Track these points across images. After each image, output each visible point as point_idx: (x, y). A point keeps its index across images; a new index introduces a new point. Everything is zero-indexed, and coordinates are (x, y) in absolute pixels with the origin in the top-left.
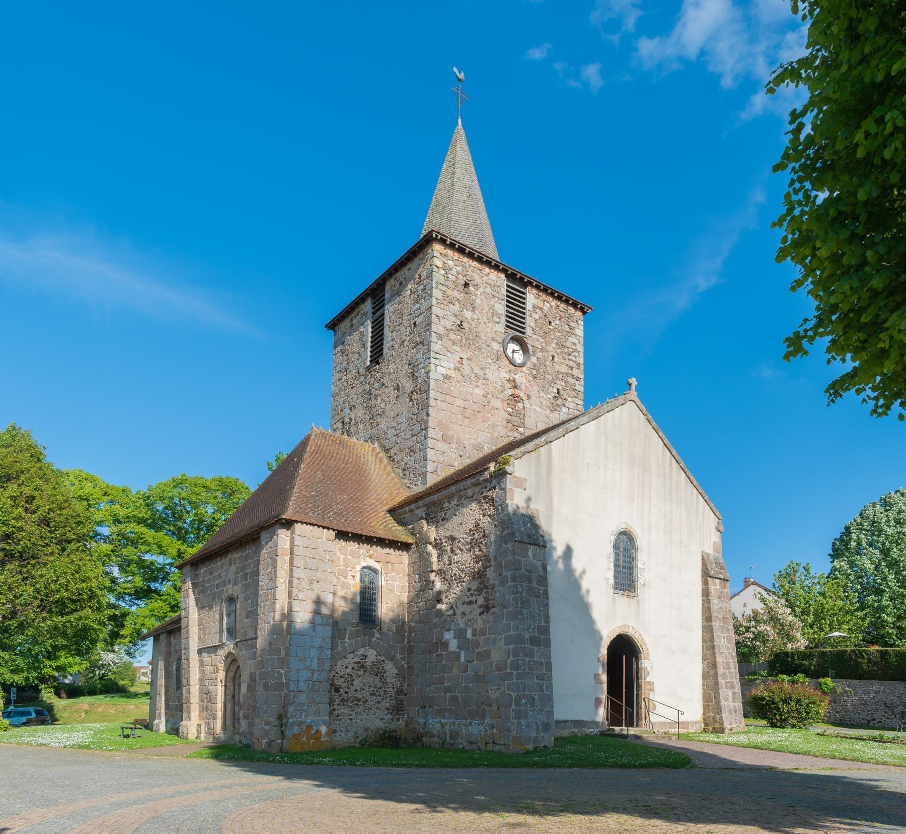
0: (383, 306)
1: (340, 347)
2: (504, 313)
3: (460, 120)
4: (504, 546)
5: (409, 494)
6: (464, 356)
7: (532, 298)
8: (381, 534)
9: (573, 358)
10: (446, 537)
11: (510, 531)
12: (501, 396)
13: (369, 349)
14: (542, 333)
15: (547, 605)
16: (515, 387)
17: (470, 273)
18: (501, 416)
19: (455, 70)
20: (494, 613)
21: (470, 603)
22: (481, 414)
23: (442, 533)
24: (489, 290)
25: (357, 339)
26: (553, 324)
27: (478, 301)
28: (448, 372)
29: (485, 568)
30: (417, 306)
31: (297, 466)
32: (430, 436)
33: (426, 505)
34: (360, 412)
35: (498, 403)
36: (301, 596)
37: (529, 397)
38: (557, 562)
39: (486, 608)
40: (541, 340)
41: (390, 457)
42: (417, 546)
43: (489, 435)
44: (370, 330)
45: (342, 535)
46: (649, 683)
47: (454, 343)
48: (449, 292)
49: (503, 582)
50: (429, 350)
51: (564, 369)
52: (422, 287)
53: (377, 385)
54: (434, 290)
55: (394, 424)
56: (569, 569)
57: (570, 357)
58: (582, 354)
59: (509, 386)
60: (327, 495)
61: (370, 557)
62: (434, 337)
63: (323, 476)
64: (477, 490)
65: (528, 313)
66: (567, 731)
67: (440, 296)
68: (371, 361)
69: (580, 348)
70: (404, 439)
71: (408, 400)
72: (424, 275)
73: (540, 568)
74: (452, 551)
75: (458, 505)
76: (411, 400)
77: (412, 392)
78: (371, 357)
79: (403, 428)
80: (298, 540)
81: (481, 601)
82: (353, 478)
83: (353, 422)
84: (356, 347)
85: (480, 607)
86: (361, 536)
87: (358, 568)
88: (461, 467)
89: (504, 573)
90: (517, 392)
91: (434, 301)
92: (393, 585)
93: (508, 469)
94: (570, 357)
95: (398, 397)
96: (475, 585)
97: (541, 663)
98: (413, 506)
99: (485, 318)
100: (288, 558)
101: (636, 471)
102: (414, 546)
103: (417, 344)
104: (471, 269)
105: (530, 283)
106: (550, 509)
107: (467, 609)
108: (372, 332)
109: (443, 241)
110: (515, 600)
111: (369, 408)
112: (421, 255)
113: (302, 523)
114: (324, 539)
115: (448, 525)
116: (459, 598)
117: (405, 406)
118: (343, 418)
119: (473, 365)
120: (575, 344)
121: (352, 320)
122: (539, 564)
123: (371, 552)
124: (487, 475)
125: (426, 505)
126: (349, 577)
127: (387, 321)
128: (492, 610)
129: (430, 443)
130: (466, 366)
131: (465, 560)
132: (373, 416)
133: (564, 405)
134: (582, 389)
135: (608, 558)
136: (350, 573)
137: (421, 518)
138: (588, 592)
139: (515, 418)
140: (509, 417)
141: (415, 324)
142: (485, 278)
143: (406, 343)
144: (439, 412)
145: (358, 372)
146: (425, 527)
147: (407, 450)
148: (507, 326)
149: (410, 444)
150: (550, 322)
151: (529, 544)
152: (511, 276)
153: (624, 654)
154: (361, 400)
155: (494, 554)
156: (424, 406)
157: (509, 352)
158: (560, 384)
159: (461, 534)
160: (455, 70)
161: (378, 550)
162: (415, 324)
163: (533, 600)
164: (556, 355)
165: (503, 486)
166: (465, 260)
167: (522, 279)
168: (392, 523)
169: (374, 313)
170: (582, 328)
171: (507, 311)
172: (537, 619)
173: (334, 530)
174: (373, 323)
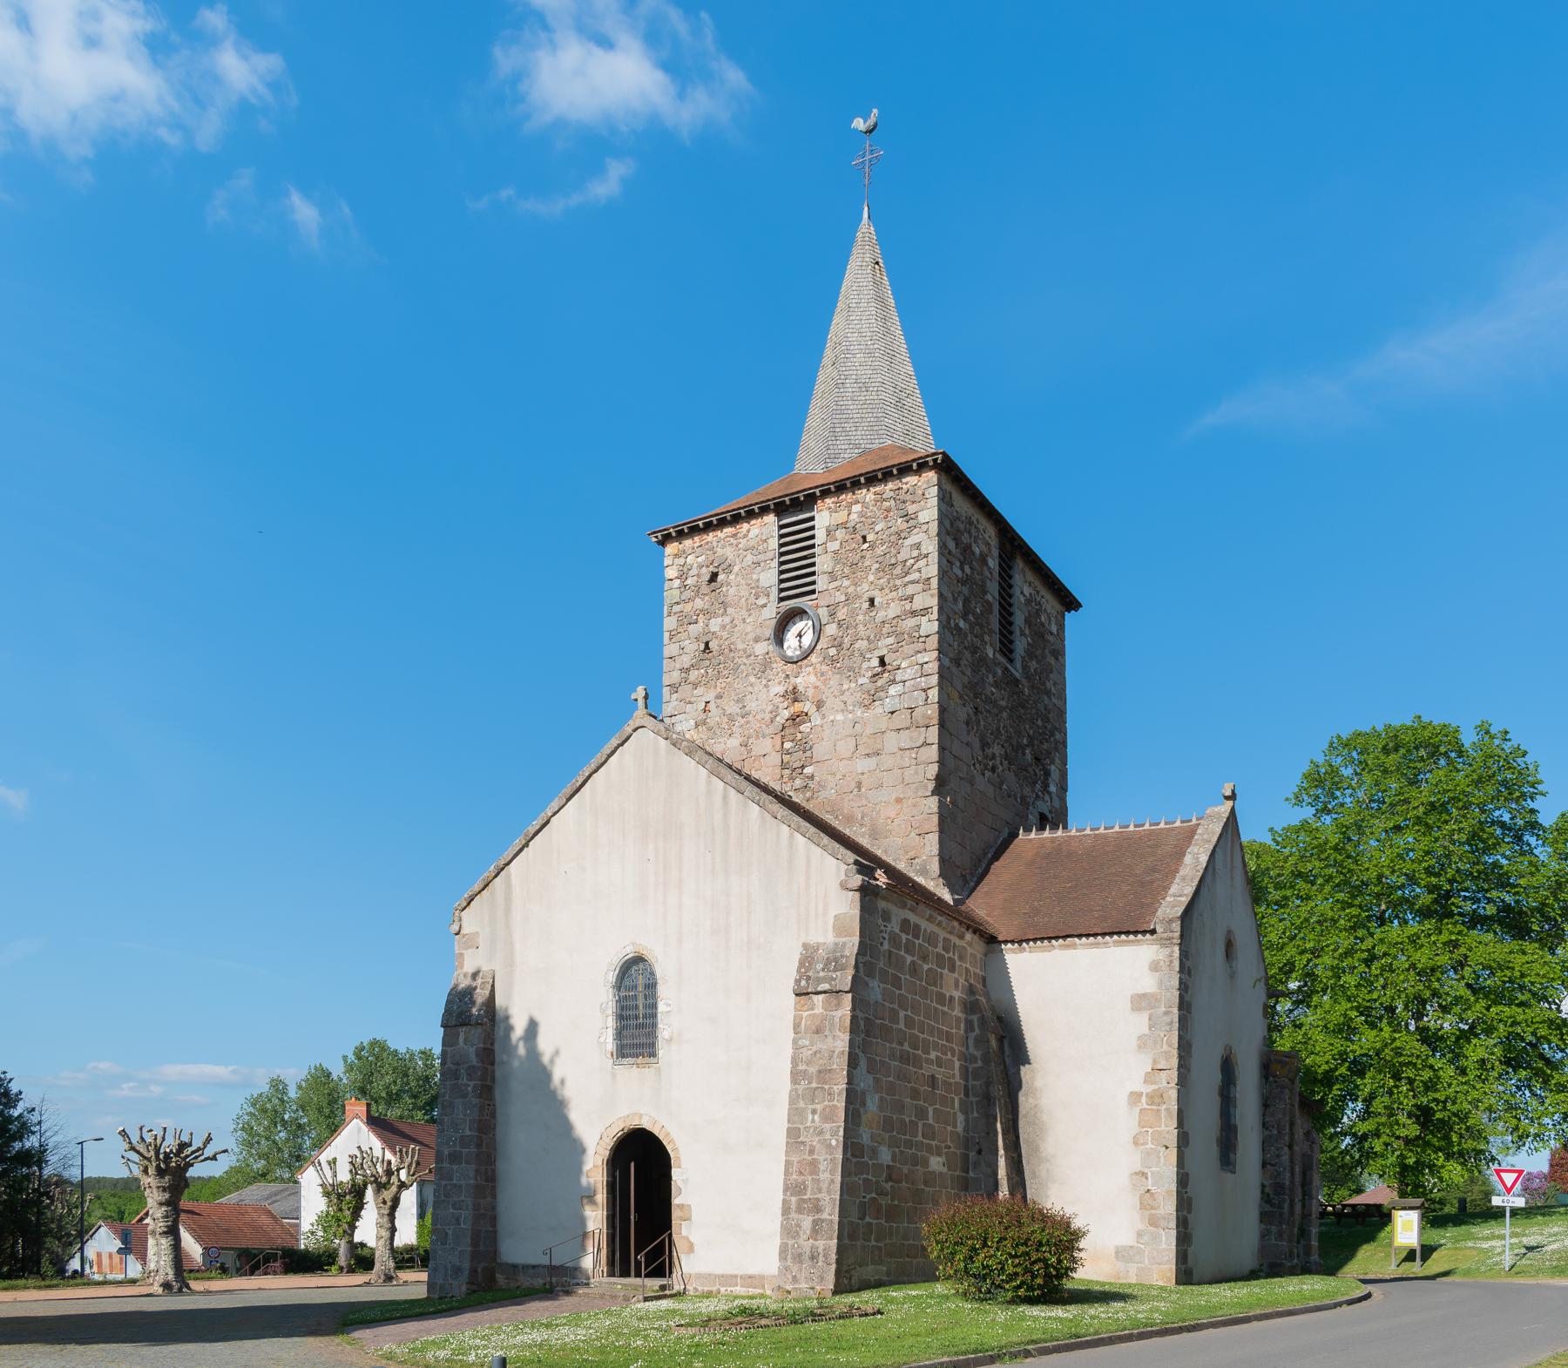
6: (710, 696)
9: (914, 576)
38: (516, 1047)
46: (681, 1206)
47: (695, 686)
56: (534, 1054)
133: (893, 682)
135: (603, 1011)
138: (563, 1082)
152: (781, 509)
153: (642, 1163)
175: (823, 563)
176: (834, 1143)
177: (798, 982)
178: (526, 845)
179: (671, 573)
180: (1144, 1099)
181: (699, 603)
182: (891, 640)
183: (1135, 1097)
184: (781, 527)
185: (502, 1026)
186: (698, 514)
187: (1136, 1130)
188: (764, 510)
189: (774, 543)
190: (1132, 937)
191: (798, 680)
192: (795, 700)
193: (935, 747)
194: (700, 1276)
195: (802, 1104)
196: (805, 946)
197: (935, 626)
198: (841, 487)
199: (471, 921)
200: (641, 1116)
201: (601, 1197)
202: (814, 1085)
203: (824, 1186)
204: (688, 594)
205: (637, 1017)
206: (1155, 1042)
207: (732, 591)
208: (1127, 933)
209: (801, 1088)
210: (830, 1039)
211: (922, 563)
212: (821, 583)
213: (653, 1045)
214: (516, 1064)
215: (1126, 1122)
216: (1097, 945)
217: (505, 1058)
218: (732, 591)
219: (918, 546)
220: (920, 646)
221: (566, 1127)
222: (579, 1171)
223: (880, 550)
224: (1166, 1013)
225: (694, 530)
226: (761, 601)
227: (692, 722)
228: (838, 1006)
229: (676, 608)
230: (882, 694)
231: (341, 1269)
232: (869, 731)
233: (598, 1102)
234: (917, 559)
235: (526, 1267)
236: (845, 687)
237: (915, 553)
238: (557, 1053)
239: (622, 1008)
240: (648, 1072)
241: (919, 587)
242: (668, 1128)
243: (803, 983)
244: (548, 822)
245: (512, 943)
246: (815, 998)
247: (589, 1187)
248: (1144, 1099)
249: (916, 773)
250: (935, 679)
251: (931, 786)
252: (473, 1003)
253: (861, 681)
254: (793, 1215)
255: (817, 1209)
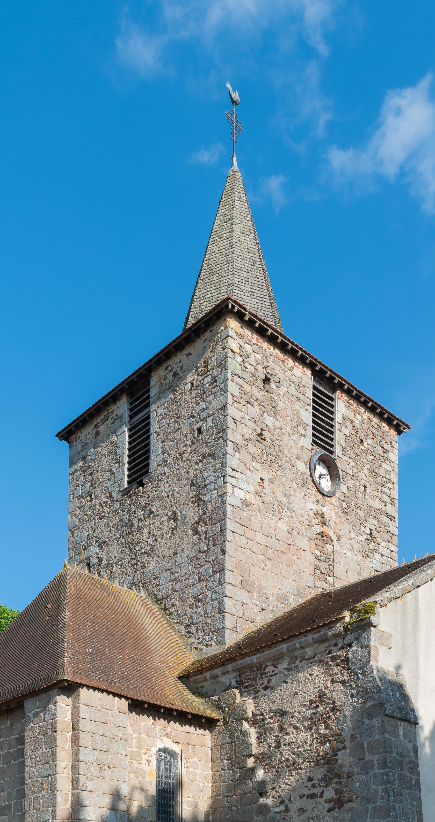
0: (148, 405)
1: (80, 464)
2: (311, 424)
3: (235, 159)
4: (367, 721)
5: (197, 658)
7: (342, 405)
8: (179, 705)
9: (386, 490)
10: (270, 711)
11: (377, 702)
12: (308, 533)
13: (127, 466)
14: (353, 455)
15: (420, 799)
16: (324, 523)
17: (271, 364)
18: (307, 560)
19: (229, 86)
20: (351, 809)
21: (312, 796)
22: (285, 556)
23: (264, 705)
24: (292, 390)
25: (106, 451)
26: (365, 444)
27: (281, 404)
28: (248, 497)
29: (335, 752)
30: (203, 405)
31: (56, 614)
32: (227, 580)
33: (239, 670)
34: (114, 550)
35: (304, 543)
36: (90, 785)
37: (339, 537)
39: (338, 803)
40: (353, 464)
41: (165, 609)
42: (226, 723)
43: (294, 583)
44: (127, 439)
45: (137, 706)
47: (254, 458)
48: (247, 388)
49: (366, 768)
50: (224, 465)
51: (377, 504)
52: (210, 379)
53: (141, 514)
54: (230, 383)
55: (171, 565)
57: (384, 489)
58: (396, 486)
59: (317, 521)
60: (105, 654)
61: (167, 736)
62: (230, 448)
63: (94, 627)
64: (322, 647)
65: (337, 426)
67: (236, 393)
68: (129, 483)
69: (395, 478)
70: (186, 585)
71: (191, 532)
72: (213, 362)
73: (411, 751)
74: (281, 729)
75: (289, 670)
76: (196, 532)
77: (197, 523)
78: (129, 476)
79: (183, 572)
80: (84, 712)
81: (329, 793)
82: (124, 634)
83: (104, 564)
84: (105, 463)
85: (329, 801)
86: (159, 707)
87: (154, 750)
88: (264, 624)
89: (368, 757)
90: (326, 529)
91: (230, 399)
92: (195, 774)
93: (374, 619)
94: (384, 489)
95: (174, 529)
96: (319, 773)
98: (217, 671)
99: (288, 428)
100: (69, 735)
102: (220, 723)
103: (204, 457)
104: (272, 358)
105: (340, 386)
106: (417, 676)
107: (308, 804)
108: (130, 443)
109: (240, 316)
110: (386, 791)
111: (130, 545)
112: (208, 334)
113: (89, 687)
114: (115, 711)
115: (275, 695)
116: (294, 790)
117: (187, 542)
118: (88, 559)
119: (276, 489)
120: (389, 473)
121: (96, 426)
122: (410, 745)
123: (169, 729)
124: (339, 627)
125: (239, 670)
126: (144, 762)
127: (154, 427)
128: (348, 806)
129: (228, 590)
130: (267, 490)
131: (302, 739)
132: (136, 556)
133: (377, 551)
134: (396, 532)
136: (145, 757)
137: (230, 687)
139: (323, 564)
140: (317, 562)
141: (199, 430)
142: (289, 373)
143: (186, 456)
144: (237, 552)
145: (110, 496)
146: (238, 699)
147: (192, 600)
148: (314, 442)
149: (195, 591)
150: (362, 441)
151: (401, 719)
152: (321, 374)
154: (115, 534)
155: (352, 732)
156: (219, 540)
157: (317, 475)
158: (373, 523)
159: (295, 707)
160: (229, 86)
161: (176, 728)
162: (199, 430)
163: (405, 791)
164: (368, 485)
165: (365, 643)
166: (266, 345)
167: (331, 379)
168: (187, 694)
169: (131, 417)
170: (396, 452)
171: (314, 422)
172: (410, 816)
173: (127, 698)
174: (130, 430)
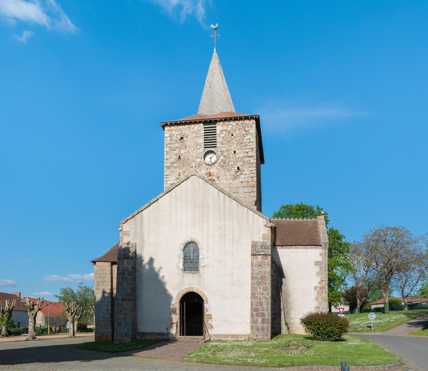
6: (181, 171)
9: (249, 147)
14: (227, 142)
24: (194, 135)
38: (145, 266)
46: (208, 315)
47: (176, 168)
56: (152, 268)
66: (154, 337)
97: (127, 309)
101: (197, 210)
133: (242, 174)
135: (179, 257)
138: (163, 277)
152: (206, 122)
175: (219, 139)
176: (268, 297)
177: (252, 251)
178: (149, 206)
179: (166, 135)
180: (318, 288)
181: (177, 145)
182: (241, 163)
183: (316, 288)
184: (205, 128)
185: (139, 260)
186: (179, 120)
187: (316, 296)
188: (200, 122)
189: (203, 132)
190: (315, 247)
191: (211, 170)
192: (210, 176)
193: (255, 193)
194: (215, 335)
195: (256, 286)
196: (252, 241)
197: (255, 161)
198: (226, 120)
199: (126, 227)
200: (193, 288)
201: (178, 312)
202: (260, 281)
203: (265, 309)
204: (172, 142)
205: (190, 259)
206: (321, 274)
207: (188, 143)
208: (314, 245)
209: (255, 281)
210: (264, 268)
211: (251, 144)
212: (218, 145)
213: (198, 267)
214: (145, 271)
215: (314, 294)
216: (305, 248)
217: (140, 269)
218: (188, 143)
219: (250, 139)
220: (250, 166)
221: (165, 291)
222: (170, 304)
223: (237, 139)
224: (324, 266)
225: (176, 124)
226: (198, 147)
227: (175, 178)
228: (266, 259)
229: (168, 145)
230: (238, 177)
231: (3, 335)
232: (234, 186)
233: (177, 284)
234: (249, 143)
235: (148, 333)
236: (227, 174)
237: (249, 141)
238: (161, 268)
239: (185, 256)
240: (196, 276)
241: (250, 150)
242: (203, 292)
243: (254, 252)
244: (158, 200)
245: (143, 235)
246: (258, 256)
247: (173, 309)
248: (318, 288)
249: (250, 199)
250: (255, 175)
251: (254, 203)
252: (130, 252)
253: (231, 173)
254: (255, 317)
255: (263, 315)
